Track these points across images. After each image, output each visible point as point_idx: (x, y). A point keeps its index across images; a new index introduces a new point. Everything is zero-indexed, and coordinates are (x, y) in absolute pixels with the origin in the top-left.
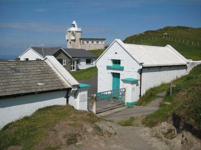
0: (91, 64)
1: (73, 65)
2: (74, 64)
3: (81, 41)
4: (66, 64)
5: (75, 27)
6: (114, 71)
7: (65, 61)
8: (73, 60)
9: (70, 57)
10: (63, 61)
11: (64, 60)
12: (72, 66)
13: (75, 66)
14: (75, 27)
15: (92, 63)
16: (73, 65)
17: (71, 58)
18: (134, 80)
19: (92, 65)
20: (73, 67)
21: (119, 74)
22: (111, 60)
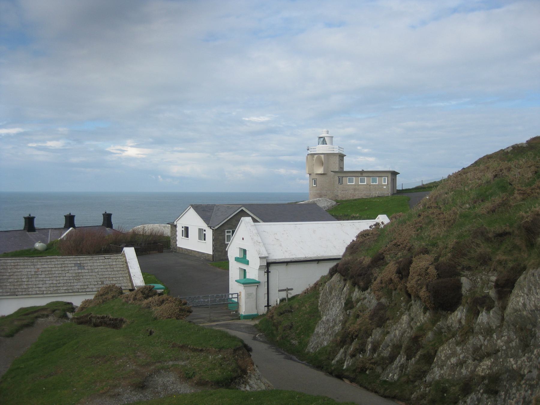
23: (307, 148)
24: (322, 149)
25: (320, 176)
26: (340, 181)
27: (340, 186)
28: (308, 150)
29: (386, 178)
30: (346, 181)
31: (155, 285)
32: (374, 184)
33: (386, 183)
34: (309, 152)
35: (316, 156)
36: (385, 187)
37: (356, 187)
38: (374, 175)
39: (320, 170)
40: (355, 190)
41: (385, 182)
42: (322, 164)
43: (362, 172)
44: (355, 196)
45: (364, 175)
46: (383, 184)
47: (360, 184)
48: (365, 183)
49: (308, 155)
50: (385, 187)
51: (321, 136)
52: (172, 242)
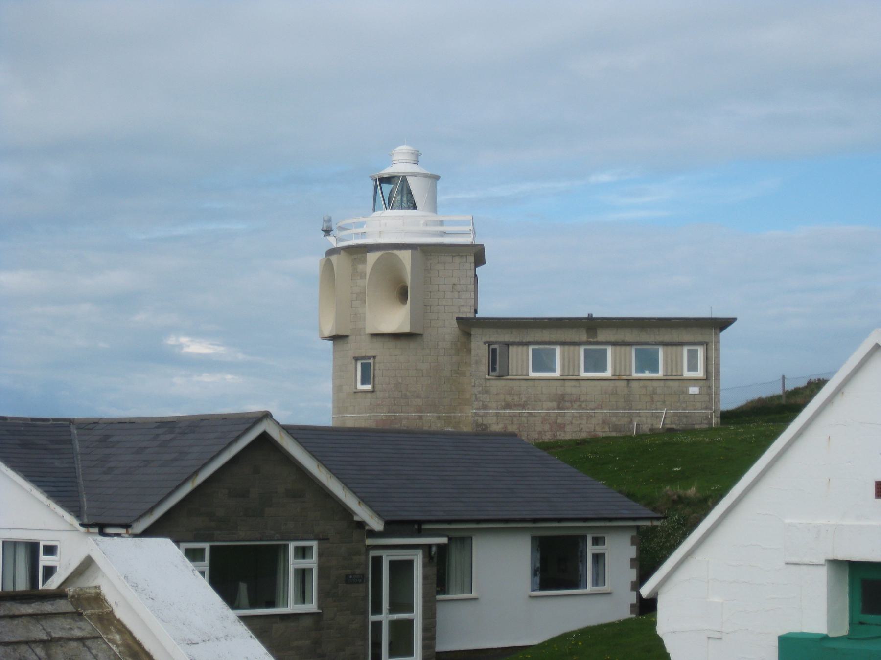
0: (590, 588)
1: (393, 609)
2: (401, 602)
3: (479, 348)
4: (323, 595)
5: (414, 207)
6: (728, 496)
7: (312, 563)
8: (387, 558)
9: (362, 513)
10: (294, 563)
11: (303, 553)
12: (385, 617)
13: (417, 615)
14: (414, 207)
15: (599, 579)
16: (393, 609)
17: (372, 534)
18: (581, 572)
19: (601, 602)
20: (393, 624)
21: (410, 653)
22: (835, 564)
23: (320, 226)
24: (390, 226)
25: (391, 344)
26: (497, 362)
27: (497, 385)
28: (327, 232)
29: (701, 351)
30: (522, 360)
31: (184, 340)
32: (647, 374)
33: (700, 373)
34: (333, 242)
35: (372, 258)
36: (694, 390)
37: (569, 388)
38: (644, 337)
39: (396, 319)
40: (561, 401)
41: (693, 367)
42: (403, 294)
43: (591, 325)
44: (562, 427)
45: (602, 336)
46: (687, 374)
47: (584, 374)
48: (608, 374)
49: (332, 252)
50: (694, 390)
51: (389, 171)
52: (859, 605)
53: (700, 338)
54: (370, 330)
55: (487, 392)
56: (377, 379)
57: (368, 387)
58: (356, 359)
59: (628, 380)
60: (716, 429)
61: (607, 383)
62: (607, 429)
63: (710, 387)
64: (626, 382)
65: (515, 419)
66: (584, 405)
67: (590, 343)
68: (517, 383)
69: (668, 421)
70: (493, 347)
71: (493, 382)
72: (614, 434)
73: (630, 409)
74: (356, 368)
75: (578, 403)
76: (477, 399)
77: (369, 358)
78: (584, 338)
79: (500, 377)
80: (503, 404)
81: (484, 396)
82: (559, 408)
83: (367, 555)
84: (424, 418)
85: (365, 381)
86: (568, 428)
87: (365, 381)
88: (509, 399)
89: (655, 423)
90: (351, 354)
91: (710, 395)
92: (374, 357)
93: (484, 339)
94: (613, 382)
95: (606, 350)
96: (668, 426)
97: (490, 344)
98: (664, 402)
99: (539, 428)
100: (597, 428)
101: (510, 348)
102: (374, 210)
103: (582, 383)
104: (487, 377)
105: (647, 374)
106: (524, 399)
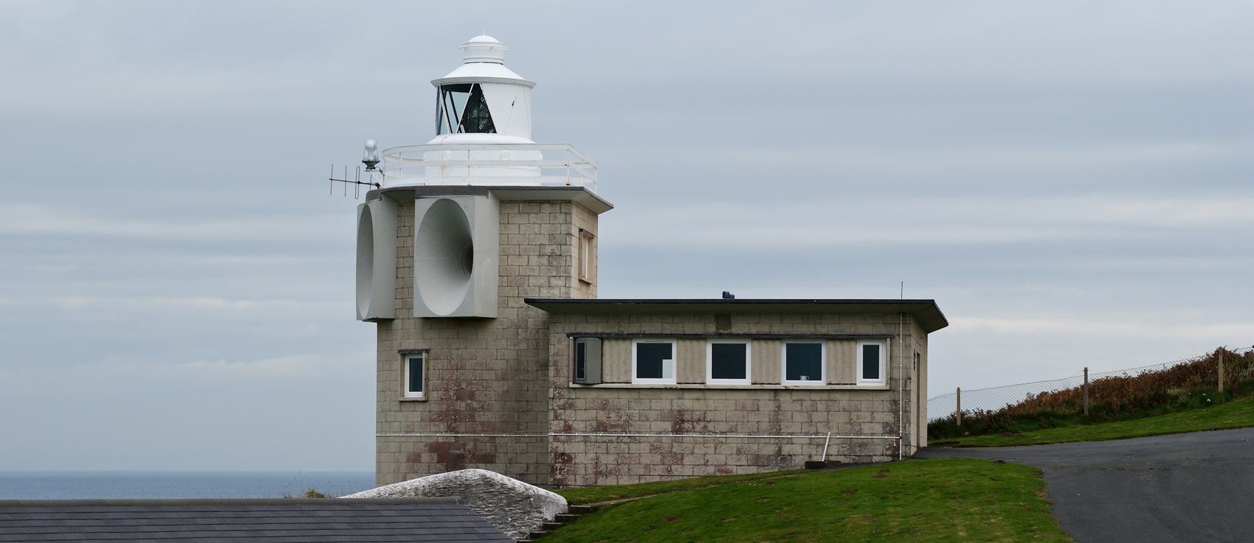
3: (561, 347)
53: (882, 329)
54: (418, 313)
55: (571, 406)
56: (431, 383)
57: (418, 395)
58: (404, 354)
59: (776, 391)
60: (913, 457)
61: (744, 395)
62: (744, 462)
63: (895, 402)
64: (772, 394)
65: (611, 446)
66: (710, 426)
67: (720, 336)
68: (615, 395)
69: (834, 451)
70: (580, 341)
71: (580, 394)
72: (753, 470)
73: (779, 433)
74: (403, 370)
75: (702, 424)
76: (556, 417)
77: (420, 352)
78: (712, 329)
79: (587, 387)
80: (594, 424)
81: (568, 412)
82: (675, 431)
83: (891, 379)
84: (498, 441)
85: (415, 386)
86: (687, 460)
87: (415, 386)
88: (602, 416)
89: (814, 453)
90: (396, 347)
91: (896, 412)
92: (427, 351)
93: (571, 328)
94: (751, 394)
95: (744, 346)
96: (833, 459)
97: (576, 336)
98: (828, 422)
99: (645, 460)
100: (730, 461)
101: (607, 344)
102: (439, 133)
103: (709, 395)
104: (571, 385)
105: (803, 383)
106: (624, 418)
